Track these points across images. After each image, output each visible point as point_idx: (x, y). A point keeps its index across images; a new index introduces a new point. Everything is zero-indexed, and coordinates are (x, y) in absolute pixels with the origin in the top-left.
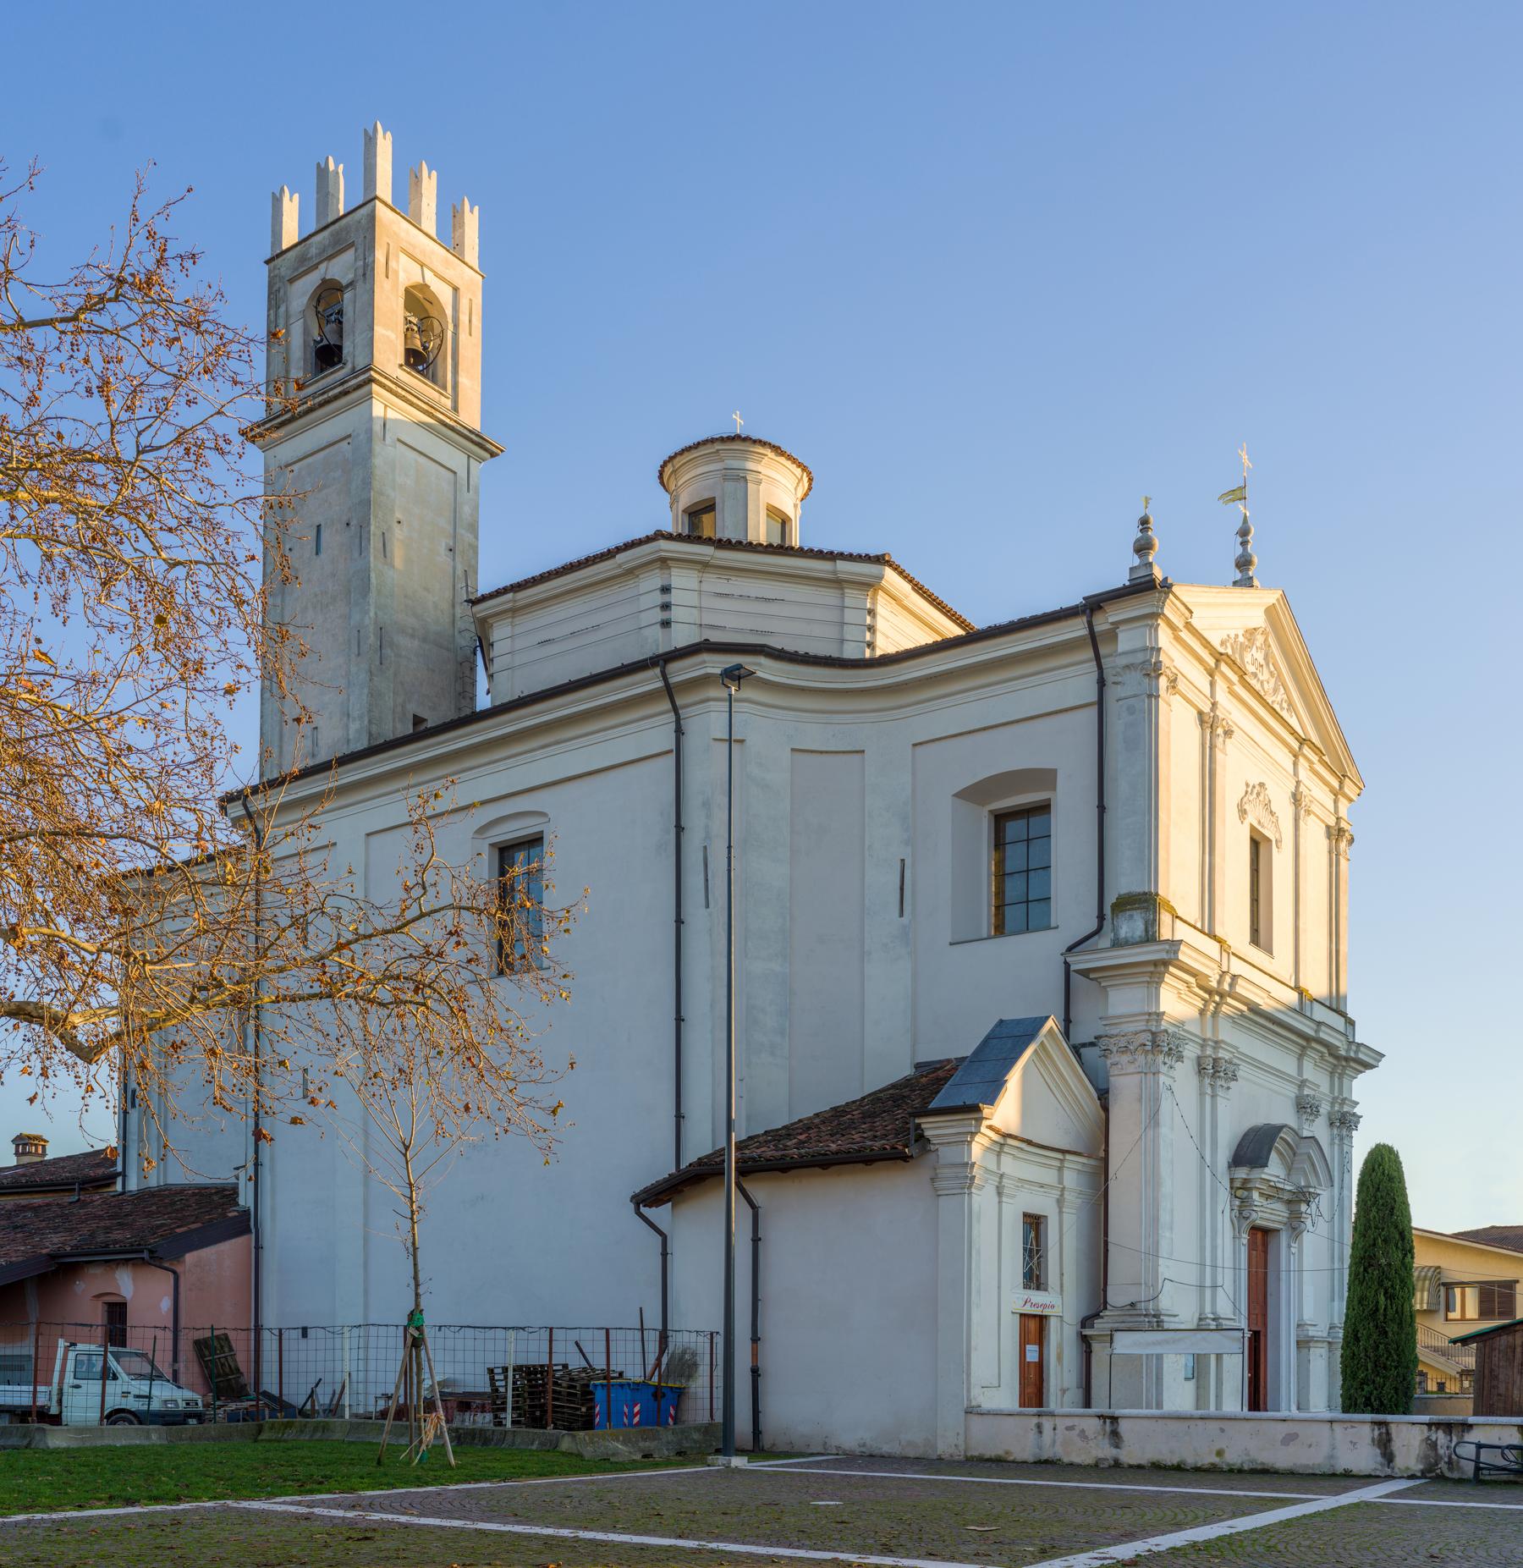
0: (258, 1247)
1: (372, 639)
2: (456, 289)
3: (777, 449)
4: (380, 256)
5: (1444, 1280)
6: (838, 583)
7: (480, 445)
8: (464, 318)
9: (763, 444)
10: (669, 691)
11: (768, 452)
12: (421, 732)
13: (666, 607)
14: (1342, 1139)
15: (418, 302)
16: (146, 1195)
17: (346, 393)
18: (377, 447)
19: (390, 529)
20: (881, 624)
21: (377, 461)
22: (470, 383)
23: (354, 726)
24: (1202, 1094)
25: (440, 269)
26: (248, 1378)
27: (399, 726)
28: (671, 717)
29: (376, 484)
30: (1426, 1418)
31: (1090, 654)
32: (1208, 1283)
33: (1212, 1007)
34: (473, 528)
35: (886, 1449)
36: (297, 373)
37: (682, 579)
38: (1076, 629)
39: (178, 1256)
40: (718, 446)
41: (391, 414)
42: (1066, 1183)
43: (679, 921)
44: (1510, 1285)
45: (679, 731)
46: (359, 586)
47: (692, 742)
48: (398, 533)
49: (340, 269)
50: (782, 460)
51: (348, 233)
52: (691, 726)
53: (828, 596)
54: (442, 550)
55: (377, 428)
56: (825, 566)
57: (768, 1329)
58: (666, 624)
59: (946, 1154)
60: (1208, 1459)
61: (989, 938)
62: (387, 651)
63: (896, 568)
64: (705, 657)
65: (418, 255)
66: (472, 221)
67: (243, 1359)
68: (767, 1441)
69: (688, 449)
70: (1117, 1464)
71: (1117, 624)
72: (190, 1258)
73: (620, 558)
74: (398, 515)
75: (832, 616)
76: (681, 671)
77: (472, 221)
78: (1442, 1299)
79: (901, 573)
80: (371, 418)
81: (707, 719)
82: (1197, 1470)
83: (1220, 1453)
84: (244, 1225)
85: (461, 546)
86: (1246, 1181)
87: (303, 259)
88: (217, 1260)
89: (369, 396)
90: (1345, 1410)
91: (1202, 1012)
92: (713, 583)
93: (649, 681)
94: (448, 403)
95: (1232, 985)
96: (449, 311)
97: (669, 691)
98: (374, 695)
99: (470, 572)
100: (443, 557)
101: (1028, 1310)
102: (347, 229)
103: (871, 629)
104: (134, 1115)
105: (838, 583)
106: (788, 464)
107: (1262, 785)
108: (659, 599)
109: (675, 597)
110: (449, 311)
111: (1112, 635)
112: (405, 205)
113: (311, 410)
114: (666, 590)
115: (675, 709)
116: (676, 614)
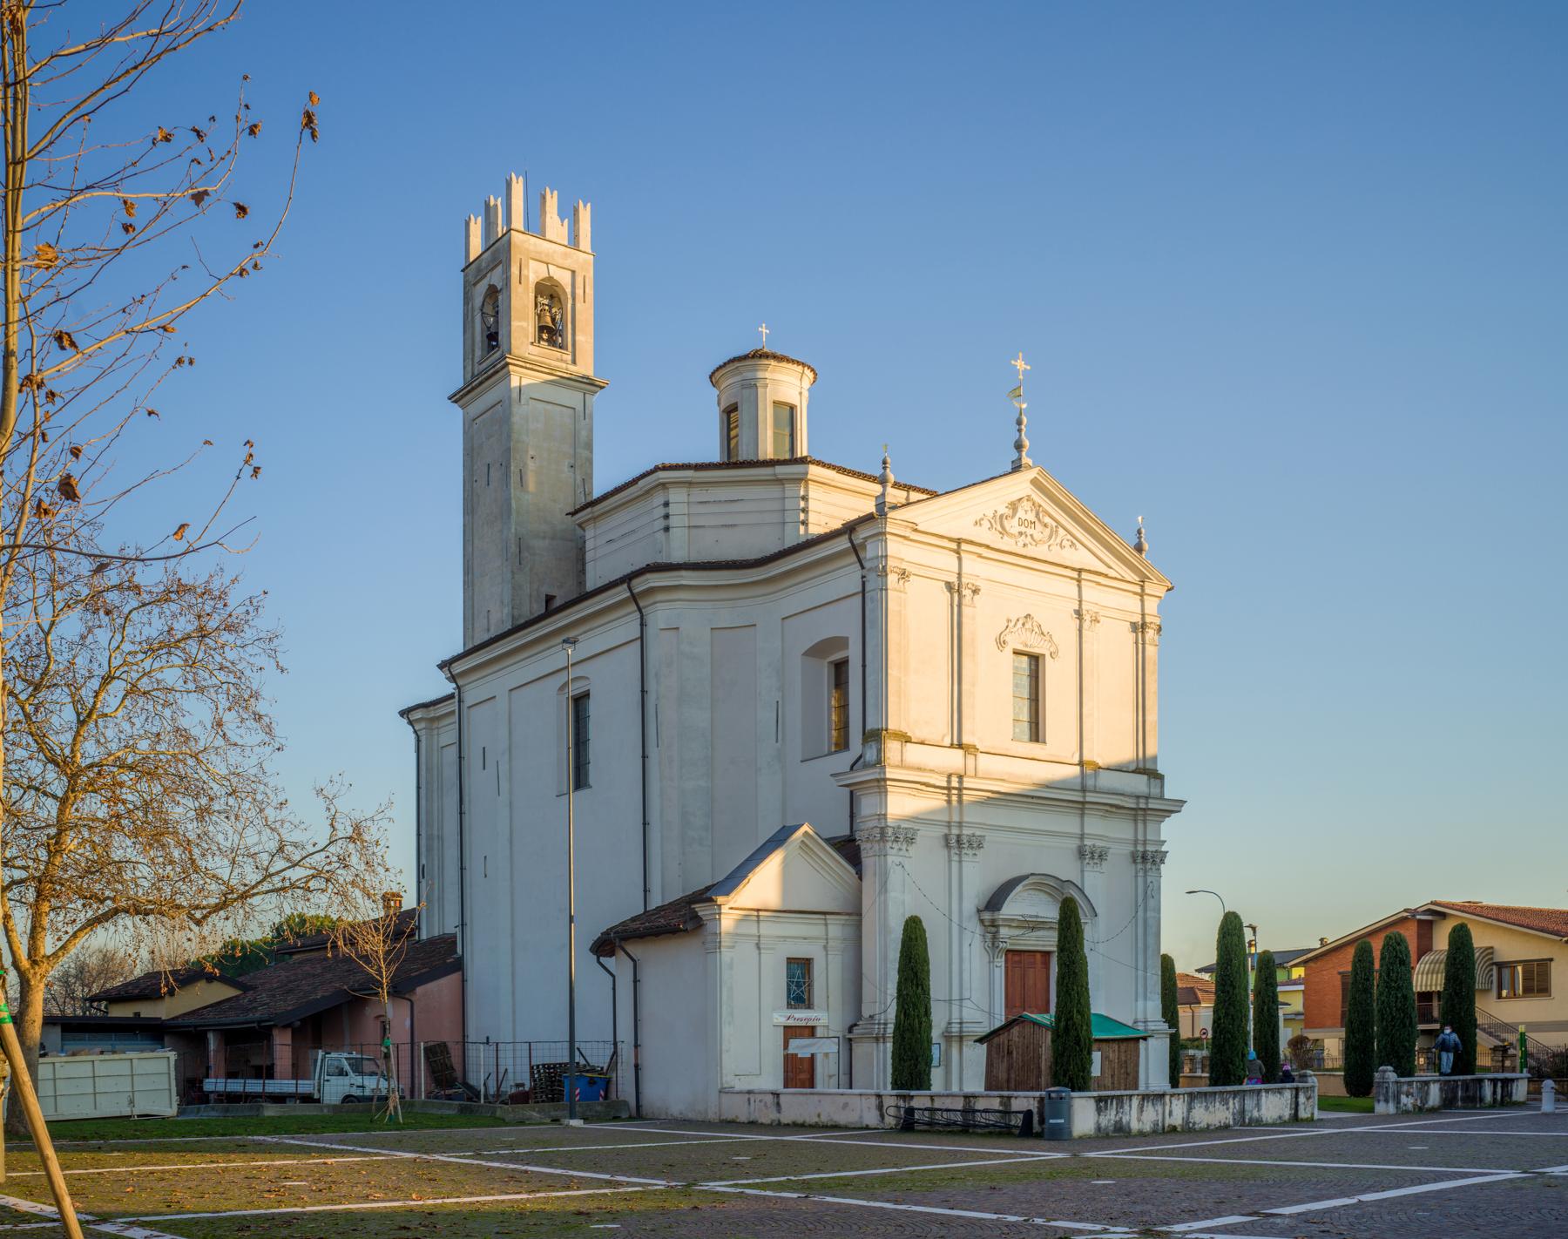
0: (463, 981)
1: (514, 549)
2: (573, 272)
3: (775, 357)
4: (515, 270)
5: (1496, 960)
6: (780, 481)
7: (589, 385)
8: (579, 291)
9: (767, 356)
10: (634, 598)
11: (773, 362)
12: (551, 608)
13: (667, 517)
14: (1145, 872)
15: (549, 292)
16: (432, 942)
17: (496, 372)
18: (515, 409)
19: (525, 464)
20: (812, 505)
21: (516, 419)
22: (585, 339)
23: (506, 611)
24: (950, 861)
25: (560, 262)
26: (459, 1074)
27: (535, 606)
28: (637, 615)
29: (515, 436)
30: (1095, 1094)
31: (854, 558)
32: (955, 996)
33: (954, 798)
34: (589, 446)
35: (691, 1116)
36: (478, 353)
37: (676, 495)
38: (843, 543)
39: (413, 990)
40: (737, 364)
41: (525, 382)
42: (831, 935)
43: (644, 757)
44: (1544, 965)
45: (642, 625)
46: (505, 510)
47: (651, 631)
48: (531, 465)
49: (495, 278)
50: (784, 364)
51: (499, 252)
52: (650, 619)
53: (774, 491)
54: (566, 469)
55: (515, 395)
56: (768, 471)
57: (645, 1039)
58: (667, 529)
59: (709, 925)
60: (815, 1120)
61: (830, 754)
62: (525, 554)
63: (819, 463)
64: (648, 576)
65: (552, 251)
66: (585, 215)
67: (455, 1060)
68: (644, 1112)
69: (720, 367)
70: (779, 1123)
71: (866, 539)
72: (419, 990)
73: (641, 483)
74: (531, 453)
75: (776, 506)
76: (640, 585)
77: (585, 215)
78: (1495, 978)
79: (824, 465)
80: (509, 389)
81: (661, 614)
82: (811, 1126)
83: (227, 1110)
84: (458, 966)
85: (582, 463)
86: (993, 921)
87: (479, 270)
88: (439, 990)
89: (508, 374)
90: (1214, 1081)
91: (949, 802)
92: (699, 494)
93: (622, 593)
94: (569, 358)
95: (961, 782)
96: (569, 290)
97: (634, 598)
98: (516, 588)
99: (587, 479)
100: (566, 473)
101: (791, 1023)
102: (497, 250)
103: (805, 510)
104: (424, 882)
105: (780, 481)
106: (790, 366)
107: (1028, 616)
108: (661, 511)
109: (672, 509)
110: (569, 290)
111: (863, 546)
112: (535, 226)
113: (481, 383)
114: (666, 504)
115: (640, 610)
116: (673, 521)
